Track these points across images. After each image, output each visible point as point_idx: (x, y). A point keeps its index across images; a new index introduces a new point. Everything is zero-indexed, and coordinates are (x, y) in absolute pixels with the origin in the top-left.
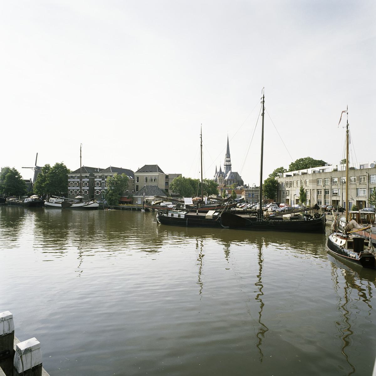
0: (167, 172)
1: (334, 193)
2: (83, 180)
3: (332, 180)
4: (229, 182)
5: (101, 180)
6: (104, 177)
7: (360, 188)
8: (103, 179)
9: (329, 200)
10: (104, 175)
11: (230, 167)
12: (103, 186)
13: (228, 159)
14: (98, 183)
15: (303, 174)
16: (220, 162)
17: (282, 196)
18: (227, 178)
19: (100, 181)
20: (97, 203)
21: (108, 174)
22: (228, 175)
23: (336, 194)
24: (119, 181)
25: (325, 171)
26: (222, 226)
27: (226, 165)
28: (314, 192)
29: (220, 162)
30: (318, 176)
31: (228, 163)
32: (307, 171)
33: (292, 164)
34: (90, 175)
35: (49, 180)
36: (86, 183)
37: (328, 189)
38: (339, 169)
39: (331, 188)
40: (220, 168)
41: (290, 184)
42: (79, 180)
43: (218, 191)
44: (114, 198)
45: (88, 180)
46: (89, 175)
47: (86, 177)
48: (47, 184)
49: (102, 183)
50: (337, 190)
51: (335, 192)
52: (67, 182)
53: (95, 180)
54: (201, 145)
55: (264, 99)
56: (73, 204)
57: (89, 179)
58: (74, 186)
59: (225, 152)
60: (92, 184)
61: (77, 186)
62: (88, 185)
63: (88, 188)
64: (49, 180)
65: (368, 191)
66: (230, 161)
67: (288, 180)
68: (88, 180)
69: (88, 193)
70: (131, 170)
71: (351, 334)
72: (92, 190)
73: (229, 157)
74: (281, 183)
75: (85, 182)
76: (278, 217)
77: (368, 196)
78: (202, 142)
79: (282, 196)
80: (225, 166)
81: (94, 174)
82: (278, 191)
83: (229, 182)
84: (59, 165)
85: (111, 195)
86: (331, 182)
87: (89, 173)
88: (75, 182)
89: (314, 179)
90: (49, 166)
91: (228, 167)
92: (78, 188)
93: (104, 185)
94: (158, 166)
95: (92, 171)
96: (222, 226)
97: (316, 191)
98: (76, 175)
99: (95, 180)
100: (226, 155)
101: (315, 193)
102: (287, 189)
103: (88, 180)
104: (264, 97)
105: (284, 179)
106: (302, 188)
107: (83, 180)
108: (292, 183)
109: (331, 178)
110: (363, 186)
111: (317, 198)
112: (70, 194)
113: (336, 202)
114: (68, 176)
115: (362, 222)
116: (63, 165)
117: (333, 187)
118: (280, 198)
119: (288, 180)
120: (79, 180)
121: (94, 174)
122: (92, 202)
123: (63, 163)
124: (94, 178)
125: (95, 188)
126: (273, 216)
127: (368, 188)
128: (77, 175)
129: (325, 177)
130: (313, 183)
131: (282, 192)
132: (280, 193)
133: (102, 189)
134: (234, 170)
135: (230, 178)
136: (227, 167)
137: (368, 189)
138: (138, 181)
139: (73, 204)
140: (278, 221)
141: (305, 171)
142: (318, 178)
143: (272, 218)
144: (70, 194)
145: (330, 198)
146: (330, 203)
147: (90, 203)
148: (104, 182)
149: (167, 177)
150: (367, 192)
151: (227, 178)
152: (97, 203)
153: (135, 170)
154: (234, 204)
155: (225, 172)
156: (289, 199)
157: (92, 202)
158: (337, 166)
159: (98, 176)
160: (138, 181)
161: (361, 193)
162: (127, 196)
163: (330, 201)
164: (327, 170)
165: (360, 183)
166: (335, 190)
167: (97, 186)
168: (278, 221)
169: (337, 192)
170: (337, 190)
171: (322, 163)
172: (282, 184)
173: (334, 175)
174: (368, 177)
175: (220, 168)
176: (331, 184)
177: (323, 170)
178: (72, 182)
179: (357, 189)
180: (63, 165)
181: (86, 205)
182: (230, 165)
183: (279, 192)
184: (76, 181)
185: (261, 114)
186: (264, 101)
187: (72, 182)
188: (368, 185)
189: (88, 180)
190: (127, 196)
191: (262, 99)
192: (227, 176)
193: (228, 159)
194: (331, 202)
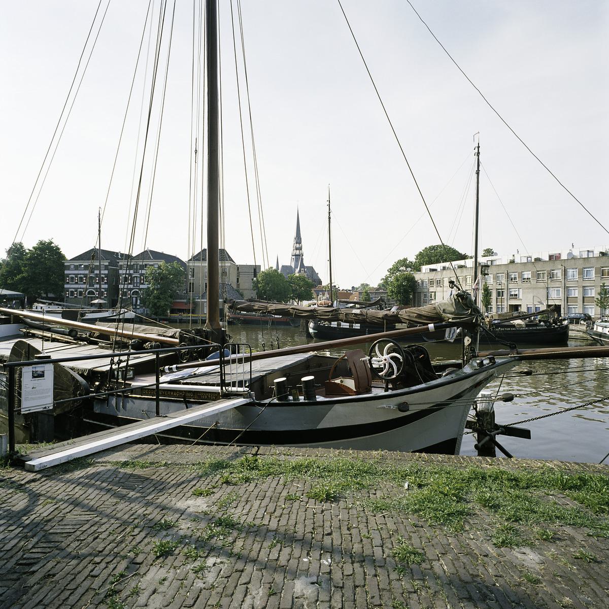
0: (238, 262)
5: (87, 272)
6: (138, 268)
7: (552, 288)
8: (92, 272)
10: (137, 265)
12: (137, 283)
13: (298, 246)
15: (461, 267)
19: (86, 276)
21: (155, 263)
23: (516, 295)
24: (170, 274)
25: (495, 263)
26: (425, 338)
27: (295, 255)
31: (298, 253)
32: (465, 263)
33: (420, 255)
34: (110, 264)
35: (27, 271)
38: (517, 260)
42: (87, 272)
43: (312, 293)
44: (163, 303)
45: (107, 273)
46: (107, 264)
48: (23, 278)
49: (134, 277)
50: (517, 290)
51: (513, 293)
54: (330, 218)
55: (478, 150)
56: (86, 313)
57: (108, 270)
58: (77, 283)
59: (294, 234)
60: (114, 280)
61: (85, 283)
62: (106, 281)
64: (27, 271)
65: (565, 291)
66: (300, 249)
67: (432, 276)
68: (107, 273)
69: (106, 295)
70: (178, 256)
71: (79, 564)
72: (114, 290)
73: (300, 243)
74: (419, 281)
76: (506, 323)
77: (565, 298)
78: (330, 213)
80: (294, 257)
82: (414, 293)
84: (44, 244)
85: (158, 298)
86: (507, 278)
87: (106, 260)
88: (79, 276)
90: (20, 245)
91: (298, 257)
93: (138, 281)
94: (151, 251)
95: (112, 256)
96: (425, 338)
100: (295, 238)
102: (431, 290)
104: (479, 147)
105: (439, 273)
106: (486, 285)
108: (441, 281)
110: (557, 284)
111: (497, 303)
113: (516, 308)
114: (66, 264)
116: (52, 245)
117: (510, 286)
119: (432, 276)
123: (53, 241)
126: (499, 323)
127: (565, 287)
129: (498, 271)
131: (422, 294)
132: (418, 296)
133: (134, 289)
137: (564, 289)
139: (87, 314)
140: (509, 329)
141: (433, 266)
142: (602, 265)
143: (497, 325)
144: (68, 297)
148: (136, 277)
149: (238, 268)
150: (562, 293)
153: (185, 258)
155: (293, 266)
158: (514, 256)
159: (72, 267)
161: (553, 294)
162: (185, 301)
165: (602, 278)
167: (145, 283)
168: (509, 329)
169: (517, 293)
170: (517, 290)
172: (423, 282)
173: (512, 268)
174: (565, 271)
176: (507, 281)
178: (74, 276)
179: (547, 288)
180: (52, 245)
181: (115, 314)
183: (416, 294)
184: (81, 274)
186: (478, 153)
187: (74, 276)
188: (565, 282)
190: (185, 301)
191: (477, 149)
193: (298, 246)
194: (507, 307)
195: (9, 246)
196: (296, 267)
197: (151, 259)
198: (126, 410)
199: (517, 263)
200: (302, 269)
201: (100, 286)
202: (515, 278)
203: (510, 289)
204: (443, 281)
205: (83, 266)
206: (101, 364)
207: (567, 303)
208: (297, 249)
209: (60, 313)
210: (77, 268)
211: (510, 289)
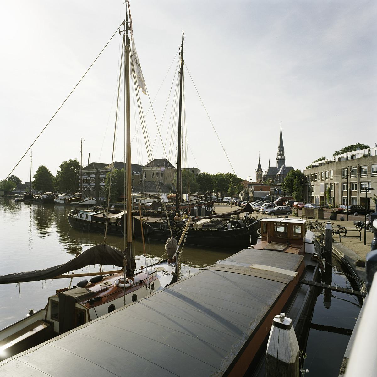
1: (363, 189)
2: (91, 176)
3: (360, 169)
4: (281, 177)
9: (356, 198)
11: (283, 162)
13: (281, 152)
14: (102, 179)
16: (259, 155)
17: (308, 192)
18: (279, 173)
20: (93, 200)
22: (281, 170)
28: (338, 187)
29: (259, 155)
30: (343, 165)
31: (281, 157)
36: (93, 179)
37: (356, 183)
39: (359, 180)
40: (259, 162)
41: (316, 177)
42: (87, 176)
47: (93, 173)
50: (367, 183)
52: (78, 178)
53: (100, 176)
61: (86, 183)
63: (94, 184)
66: (283, 154)
73: (283, 150)
75: (92, 178)
79: (308, 192)
81: (99, 170)
83: (281, 177)
87: (95, 169)
89: (339, 169)
91: (281, 161)
92: (87, 185)
97: (340, 185)
98: (85, 172)
99: (100, 176)
101: (339, 188)
103: (94, 176)
107: (91, 176)
109: (359, 166)
111: (342, 195)
112: (83, 191)
115: (146, 235)
118: (306, 195)
120: (87, 176)
121: (99, 170)
122: (88, 199)
124: (99, 174)
125: (100, 184)
128: (86, 172)
130: (337, 174)
134: (287, 164)
135: (283, 174)
136: (280, 161)
138: (145, 177)
144: (83, 191)
145: (357, 195)
146: (357, 201)
147: (85, 200)
151: (279, 173)
152: (93, 200)
154: (210, 202)
156: (314, 196)
157: (88, 199)
160: (145, 177)
163: (357, 199)
164: (356, 157)
166: (364, 183)
170: (367, 183)
171: (362, 147)
172: (308, 177)
175: (259, 162)
176: (359, 175)
177: (352, 156)
182: (284, 159)
185: (178, 70)
189: (94, 176)
192: (279, 171)
193: (281, 152)
195: (40, 165)
196: (280, 167)
197: (94, 168)
198: (328, 307)
199: (372, 156)
200: (259, 169)
201: (81, 185)
202: (366, 172)
203: (362, 182)
204: (318, 175)
205: (85, 174)
206: (48, 237)
207: (351, 196)
208: (280, 155)
209: (63, 200)
210: (89, 174)
211: (362, 182)
